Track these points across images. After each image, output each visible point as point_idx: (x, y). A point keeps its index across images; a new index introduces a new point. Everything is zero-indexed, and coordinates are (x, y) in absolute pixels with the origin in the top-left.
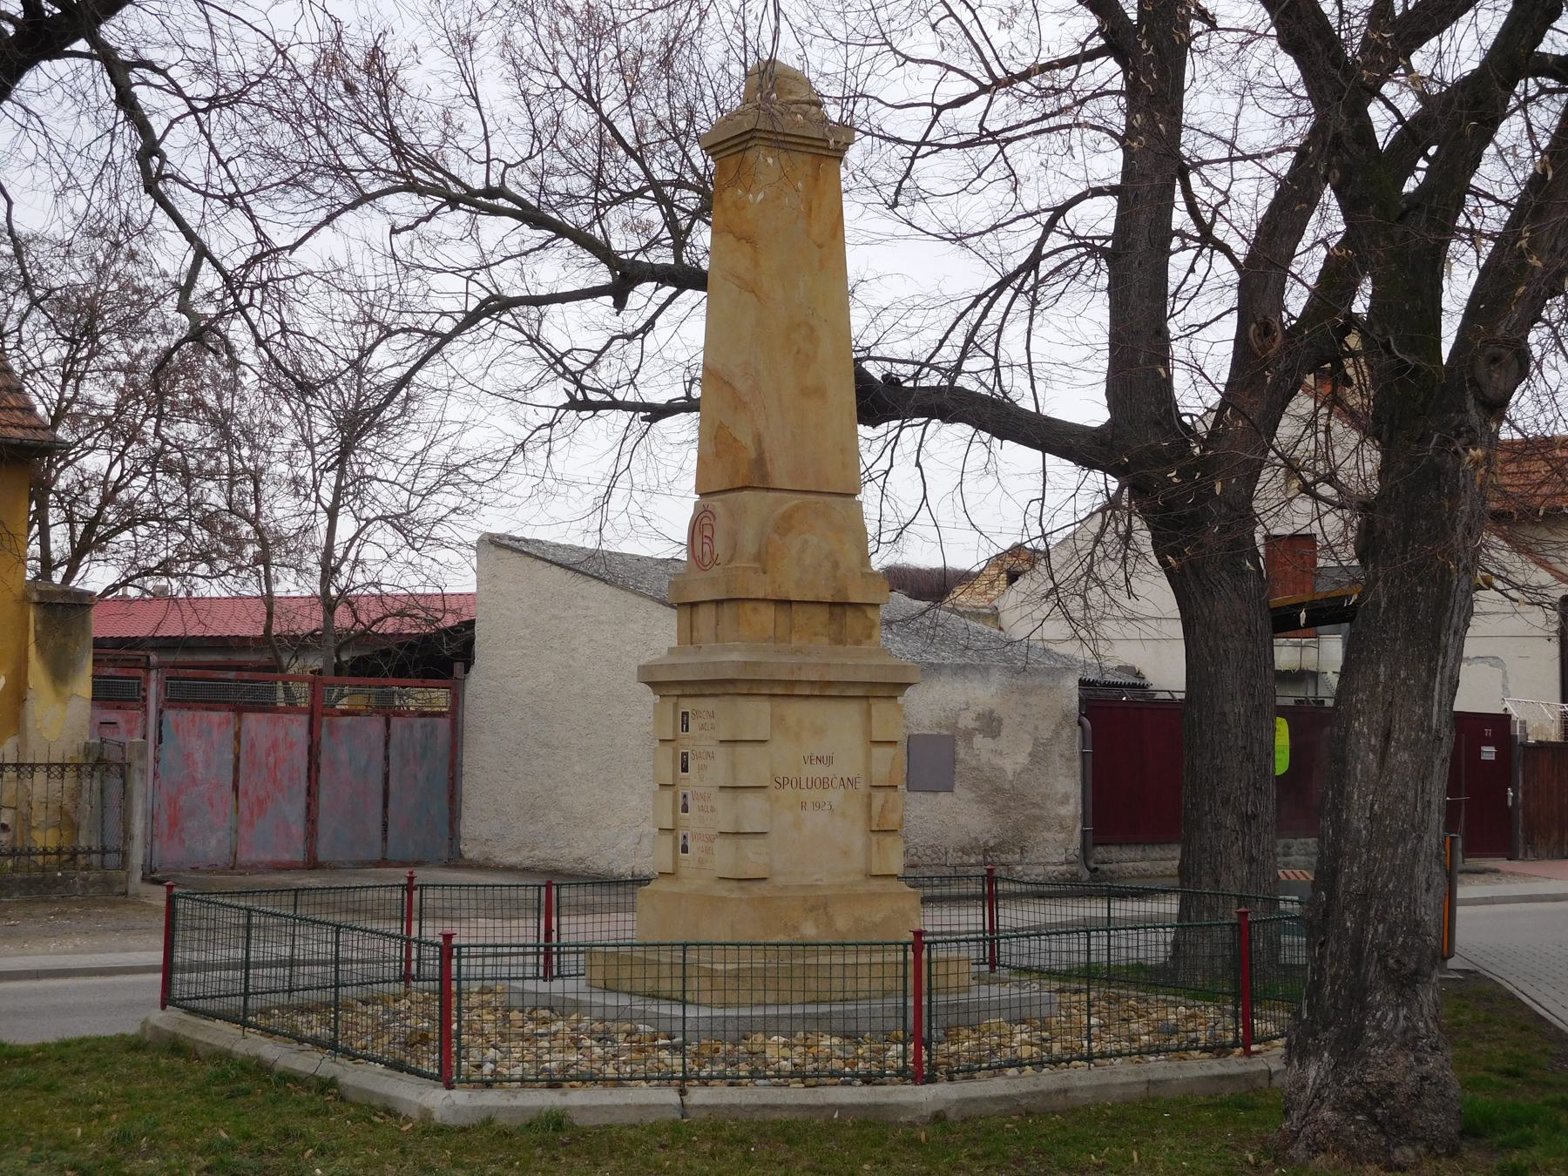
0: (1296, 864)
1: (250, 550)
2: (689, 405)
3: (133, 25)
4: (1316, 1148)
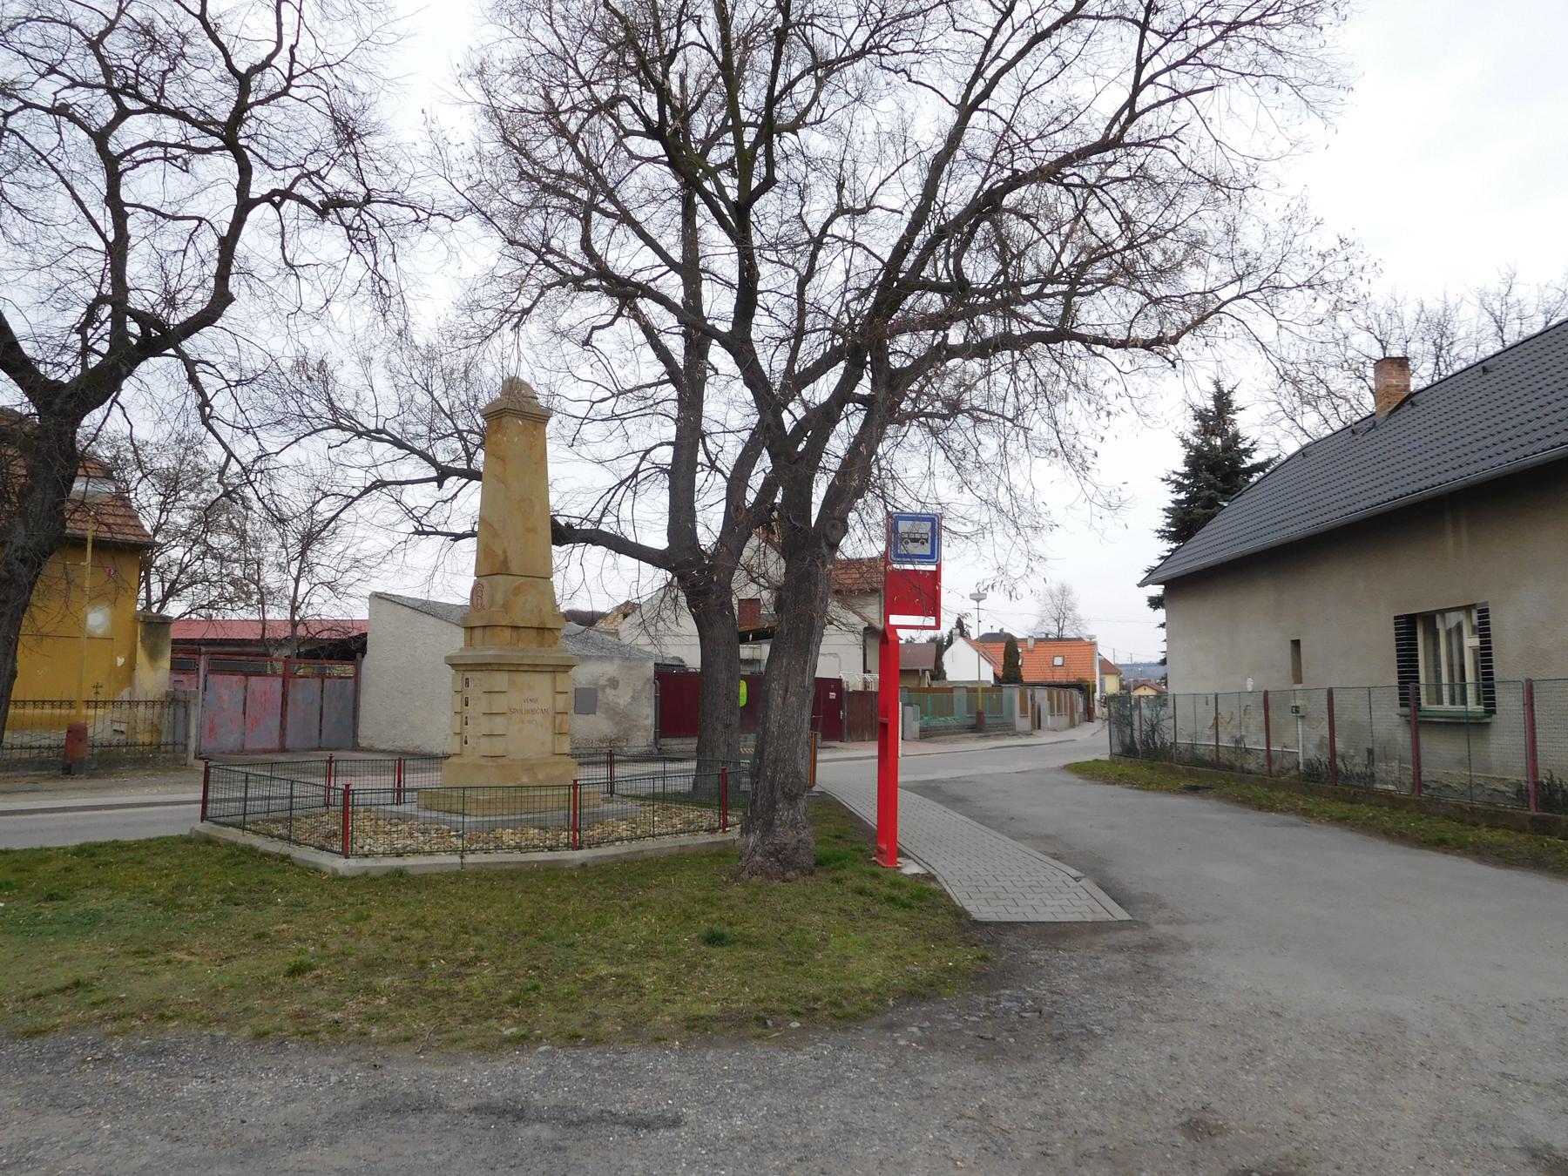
0: (748, 745)
1: (255, 597)
2: (473, 534)
3: (198, 343)
4: (753, 873)
